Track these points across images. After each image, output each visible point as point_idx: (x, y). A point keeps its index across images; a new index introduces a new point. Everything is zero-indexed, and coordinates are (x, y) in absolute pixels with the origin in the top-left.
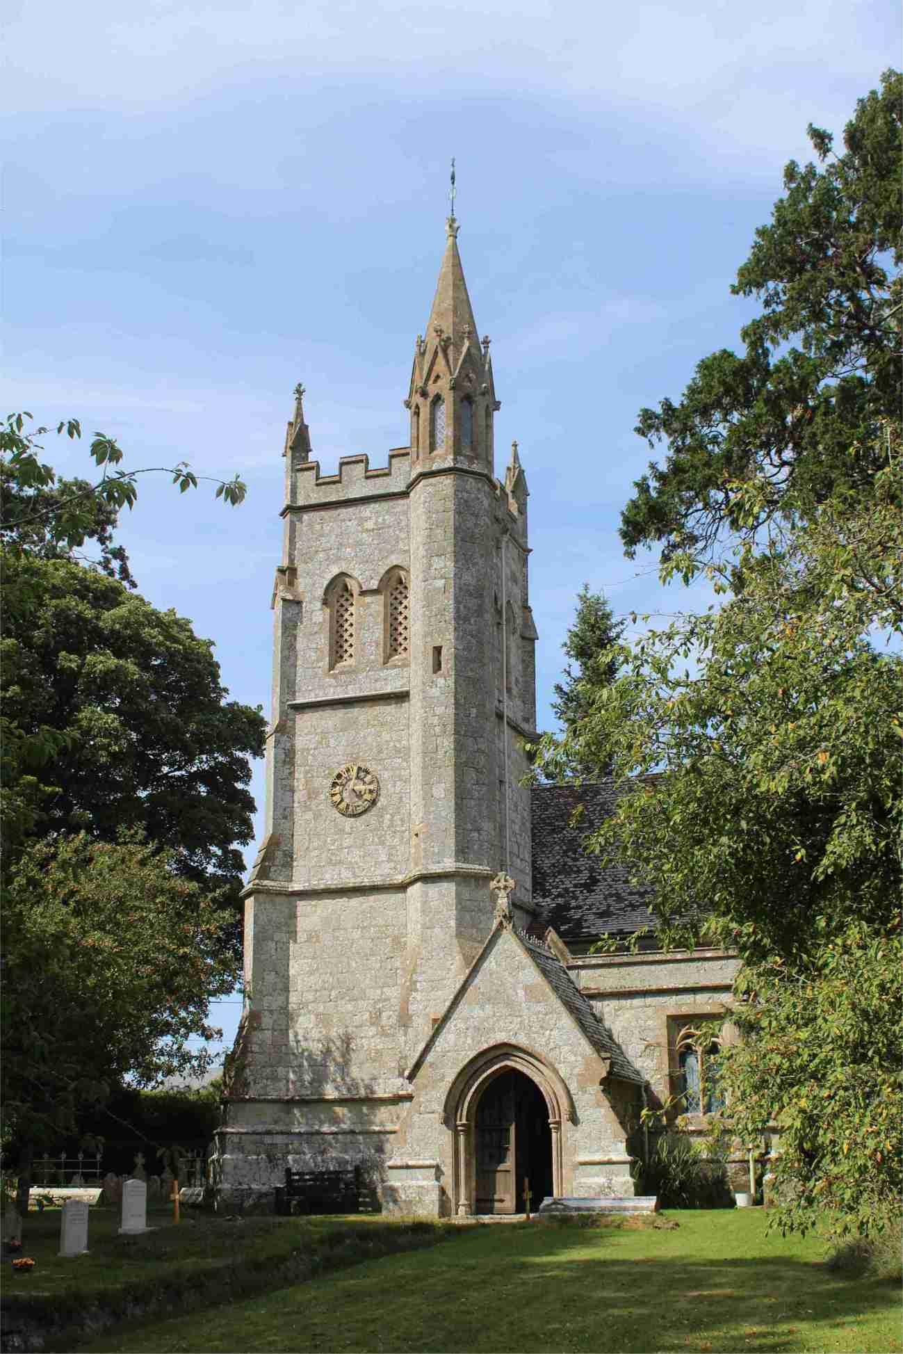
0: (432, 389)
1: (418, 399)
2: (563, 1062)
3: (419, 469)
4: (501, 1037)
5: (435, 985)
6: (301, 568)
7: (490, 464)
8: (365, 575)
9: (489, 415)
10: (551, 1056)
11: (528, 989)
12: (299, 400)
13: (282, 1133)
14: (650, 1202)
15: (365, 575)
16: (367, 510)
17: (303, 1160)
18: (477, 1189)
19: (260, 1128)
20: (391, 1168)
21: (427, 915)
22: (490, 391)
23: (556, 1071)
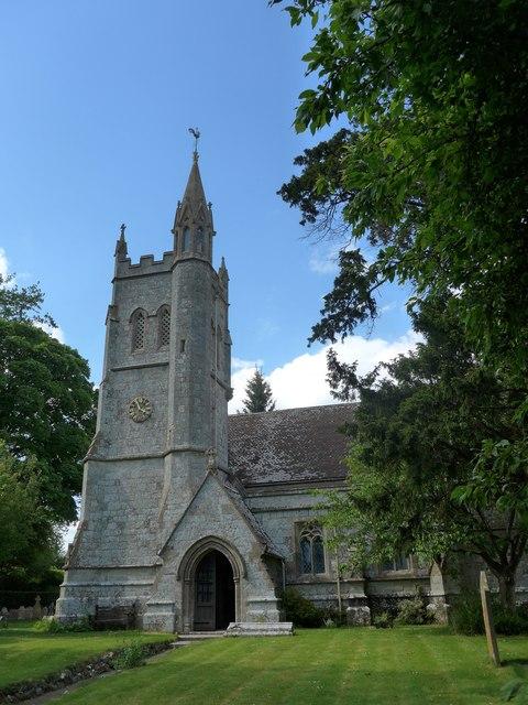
0: (185, 223)
1: (178, 229)
2: (241, 542)
3: (177, 259)
4: (209, 533)
5: (178, 506)
6: (121, 306)
7: (211, 259)
8: (150, 308)
9: (210, 237)
10: (236, 543)
11: (225, 508)
12: (123, 231)
13: (95, 585)
14: (289, 625)
15: (150, 308)
16: (152, 280)
17: (106, 600)
18: (195, 617)
19: (84, 583)
20: (248, 603)
21: (171, 473)
22: (211, 226)
23: (237, 551)
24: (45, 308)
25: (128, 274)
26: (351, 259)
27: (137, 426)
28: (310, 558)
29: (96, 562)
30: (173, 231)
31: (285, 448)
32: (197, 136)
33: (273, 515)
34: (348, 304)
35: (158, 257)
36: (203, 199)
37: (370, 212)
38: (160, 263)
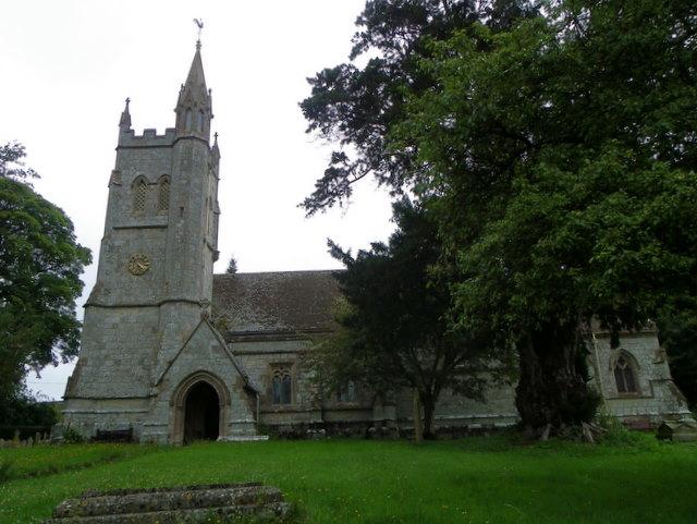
13: (93, 413)
19: (82, 411)
24: (26, 163)
25: (132, 145)
26: (339, 157)
27: (136, 278)
28: (279, 392)
29: (94, 394)
30: (175, 111)
31: (259, 304)
32: (201, 26)
33: (252, 357)
34: (330, 188)
35: (161, 132)
36: (203, 85)
37: (357, 127)
38: (138, 138)
